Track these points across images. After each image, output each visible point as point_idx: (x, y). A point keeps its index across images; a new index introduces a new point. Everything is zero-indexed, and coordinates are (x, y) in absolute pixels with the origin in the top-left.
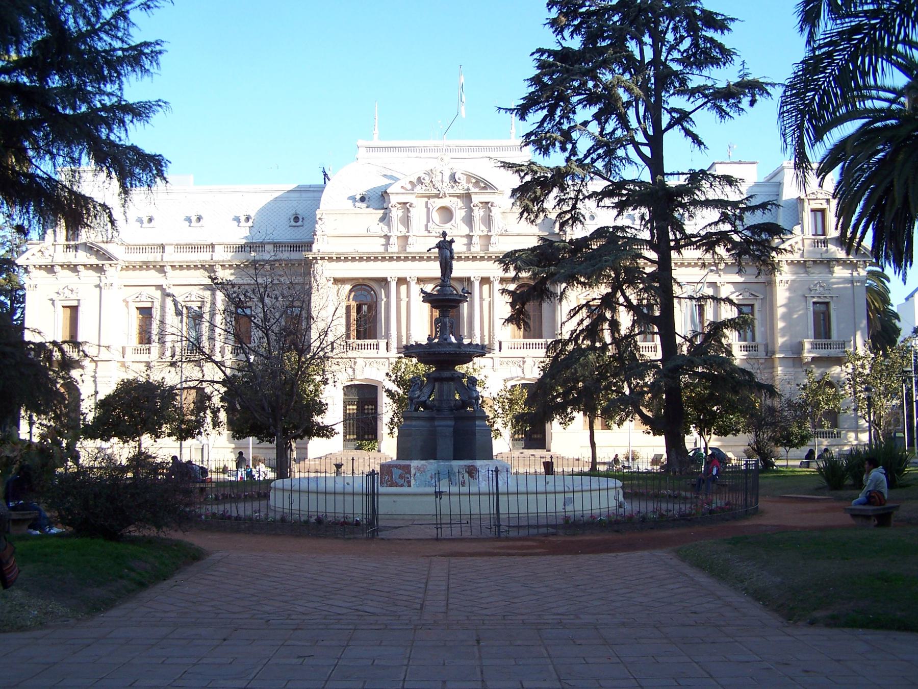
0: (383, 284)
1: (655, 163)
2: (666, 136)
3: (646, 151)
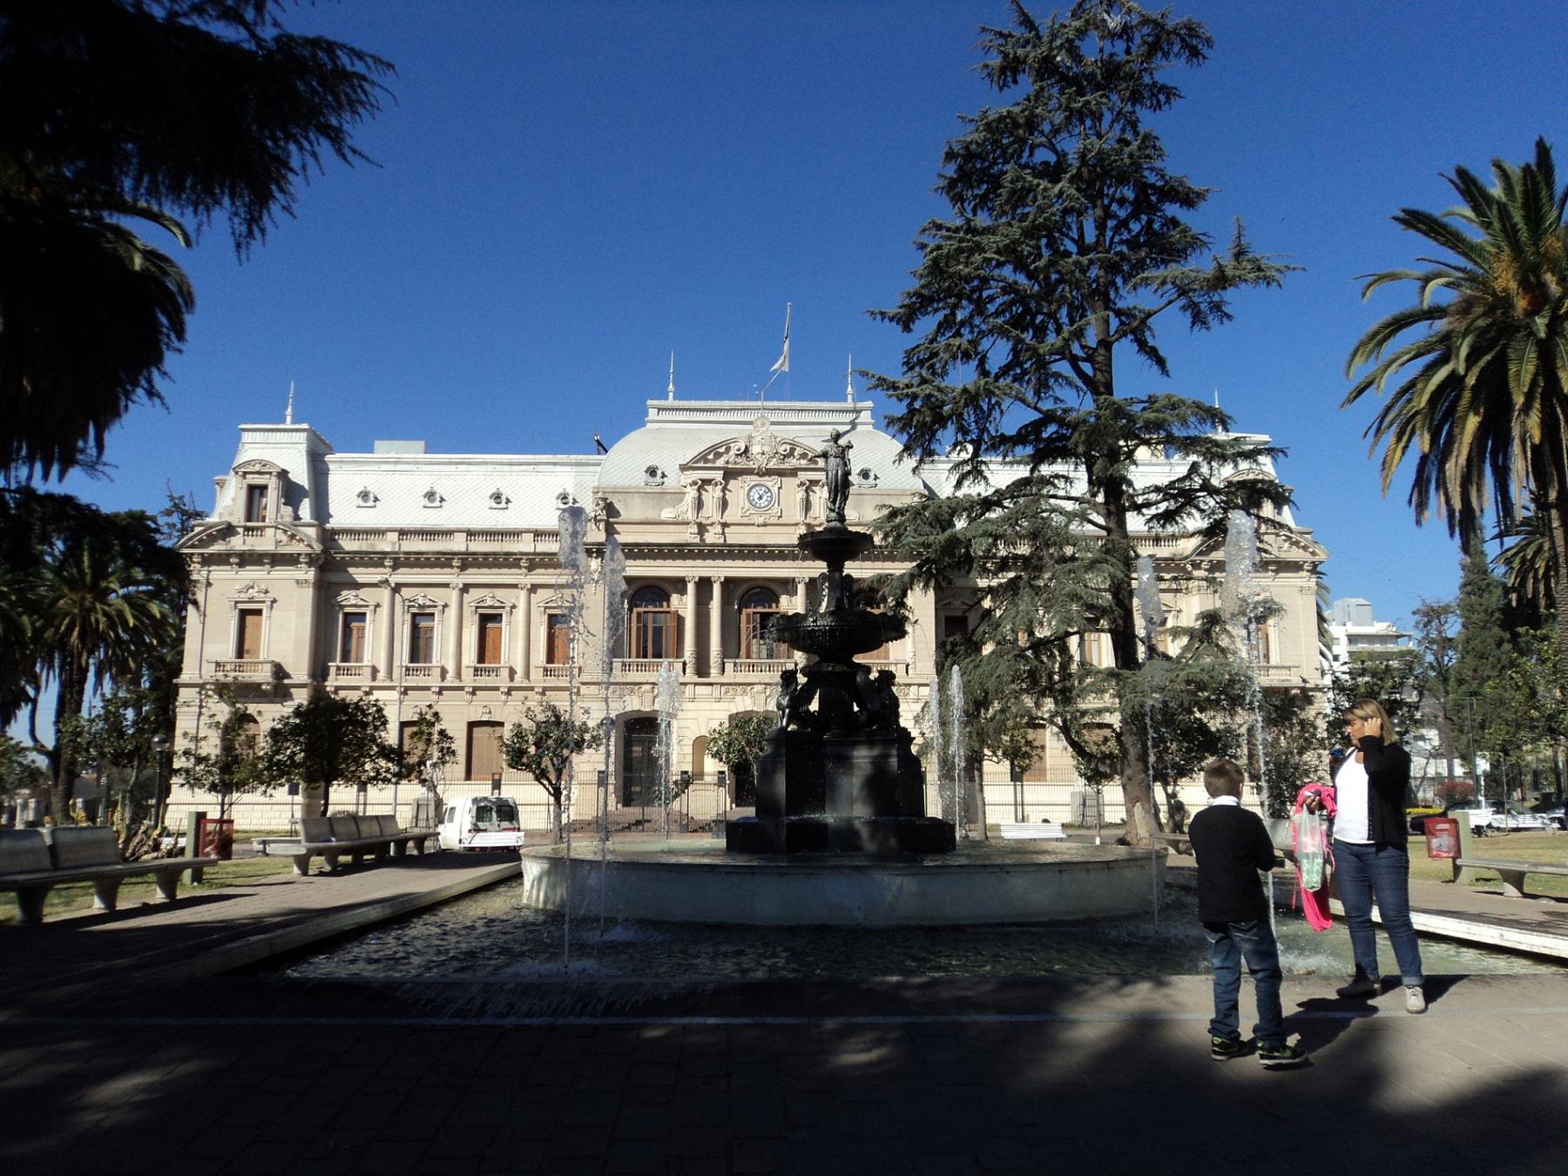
1: (1100, 386)
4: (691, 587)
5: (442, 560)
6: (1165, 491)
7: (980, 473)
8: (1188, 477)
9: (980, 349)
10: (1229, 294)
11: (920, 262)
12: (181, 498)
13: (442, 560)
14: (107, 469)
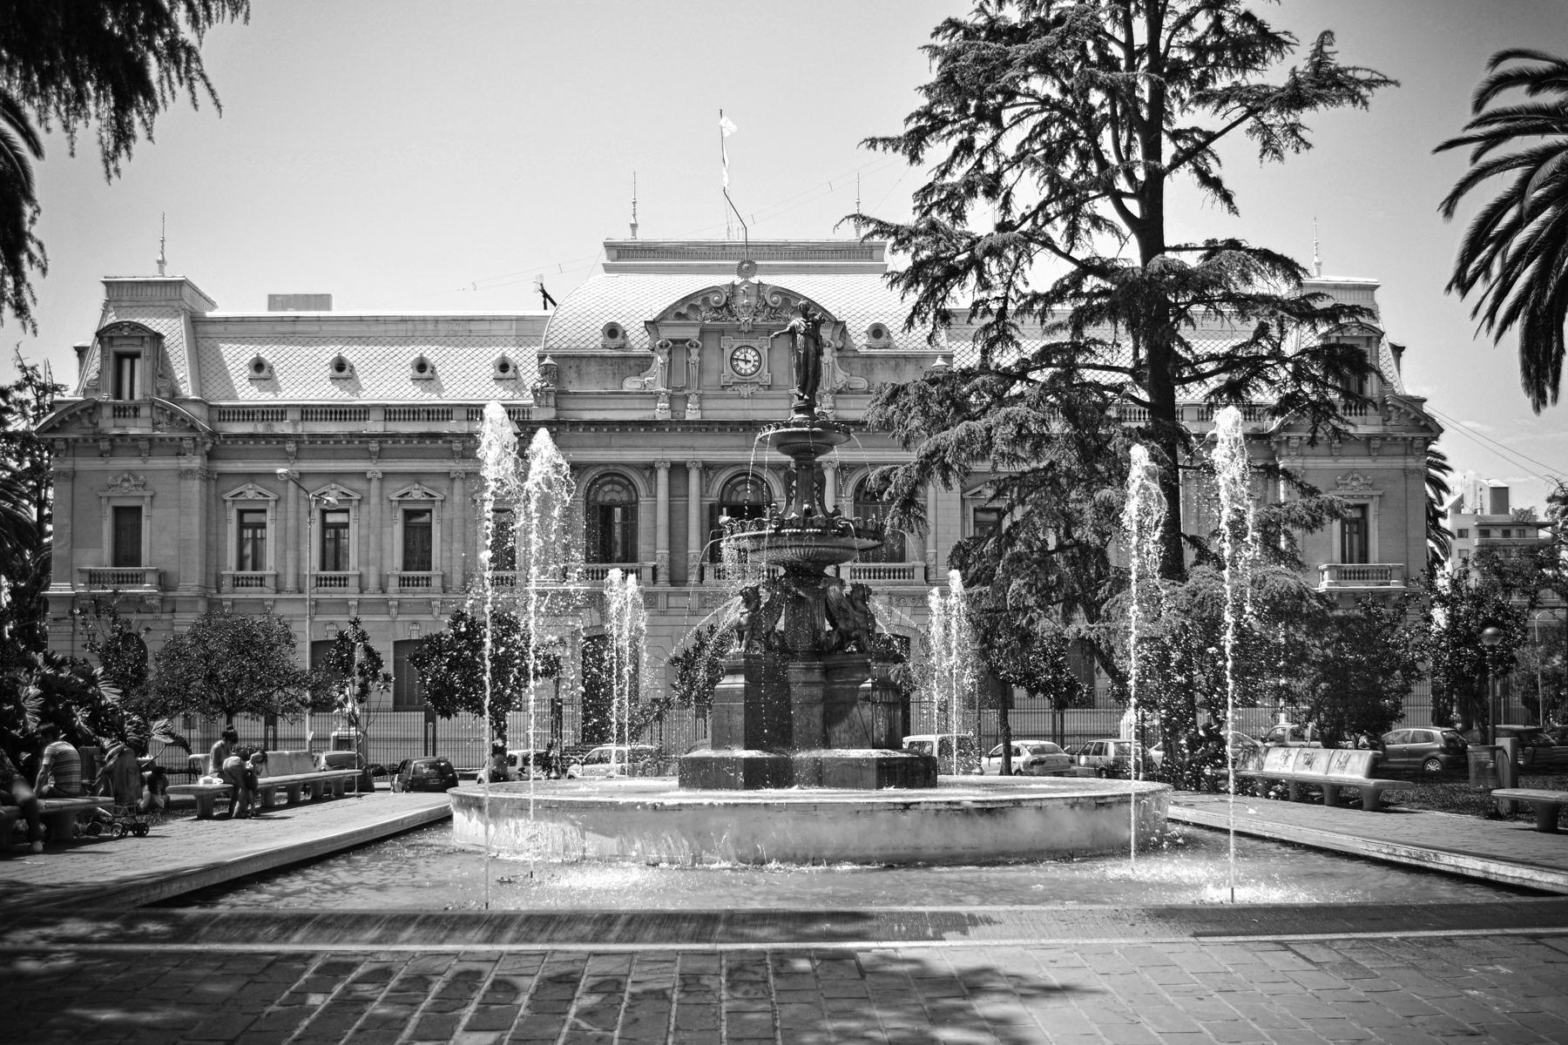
0: (647, 473)
1: (1149, 230)
2: (1170, 185)
3: (1133, 206)
4: (662, 476)
5: (359, 445)
6: (1228, 361)
7: (1011, 338)
8: (1255, 341)
9: (1003, 184)
10: (1306, 116)
11: (930, 72)
12: (33, 368)
13: (359, 445)
14: (1270, 485)
